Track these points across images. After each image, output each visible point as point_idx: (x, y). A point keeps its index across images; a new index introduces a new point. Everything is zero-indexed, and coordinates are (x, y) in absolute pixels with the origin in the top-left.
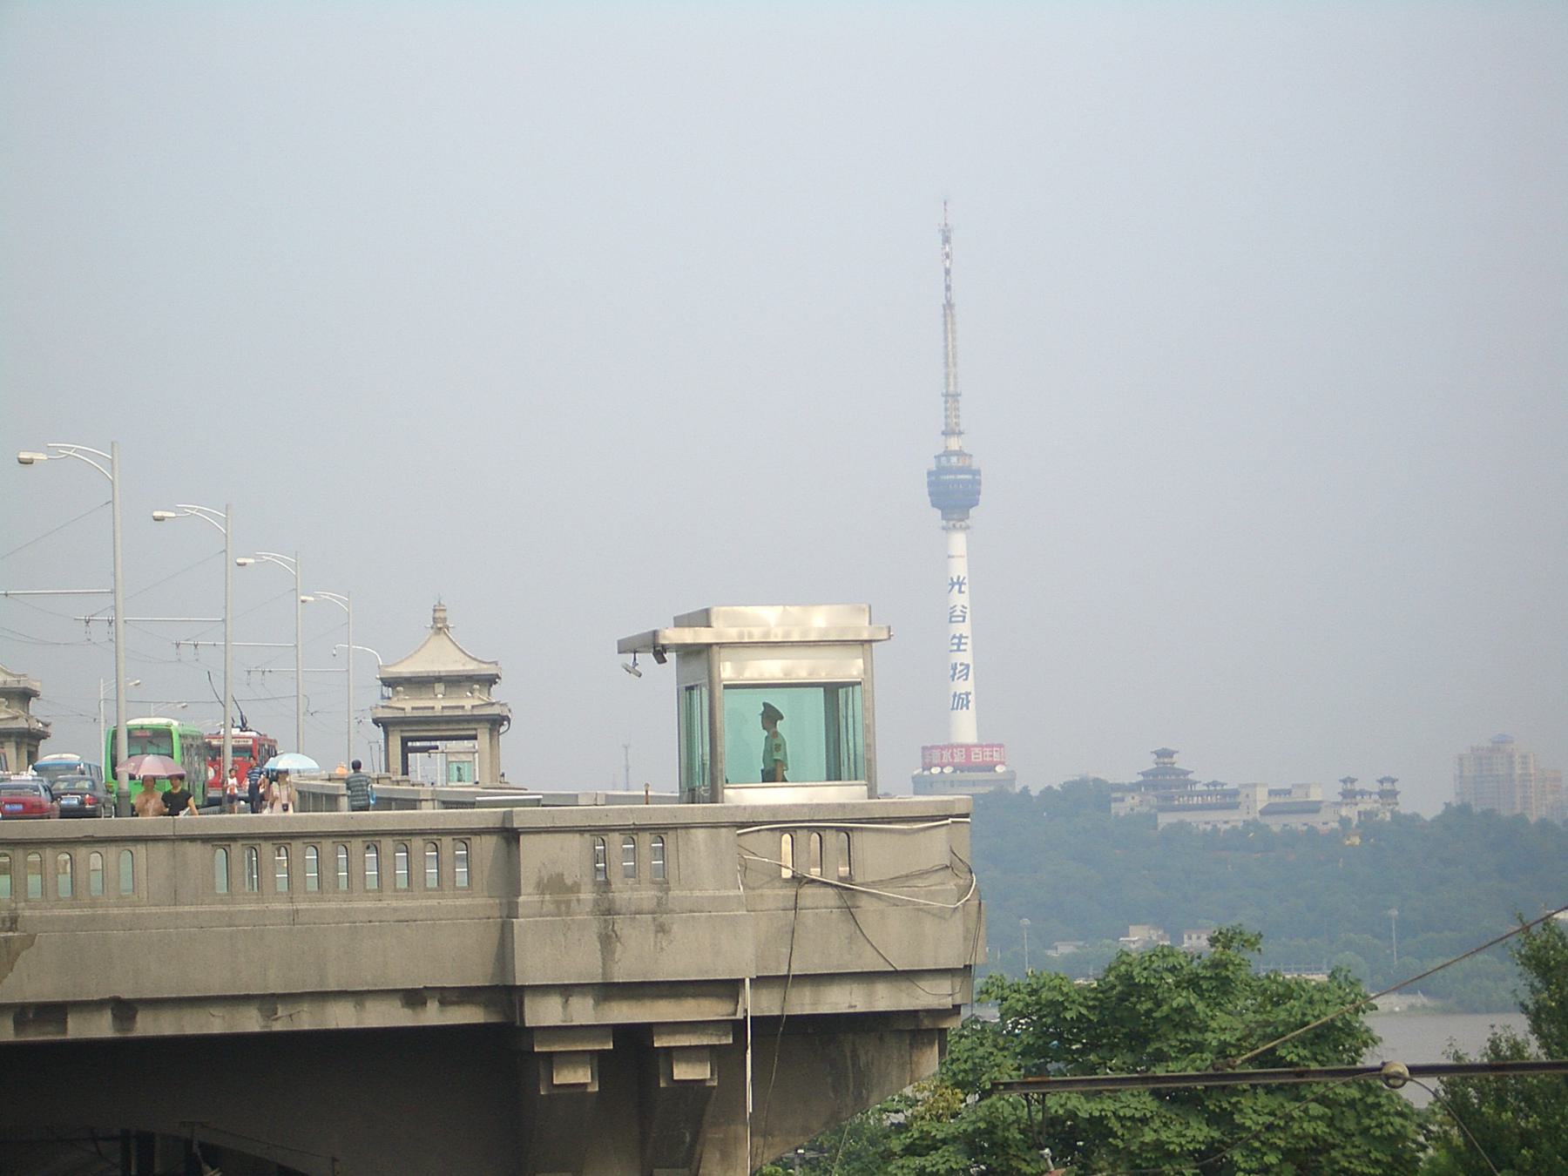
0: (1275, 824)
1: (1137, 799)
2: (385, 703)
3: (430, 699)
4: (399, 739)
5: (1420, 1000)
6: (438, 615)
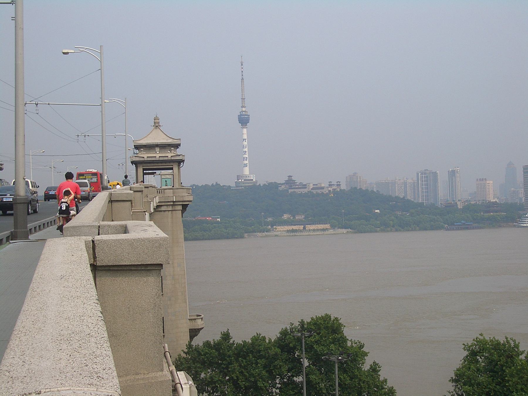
0: (314, 192)
1: (284, 186)
2: (136, 155)
3: (154, 153)
4: (142, 169)
5: (349, 230)
6: (156, 121)
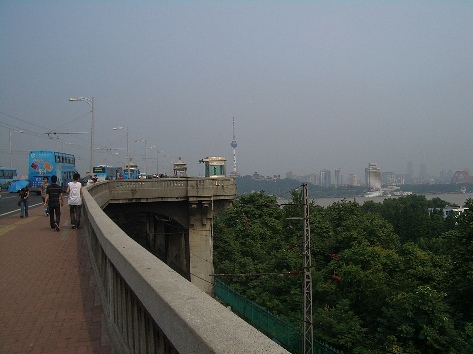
5: (282, 198)
